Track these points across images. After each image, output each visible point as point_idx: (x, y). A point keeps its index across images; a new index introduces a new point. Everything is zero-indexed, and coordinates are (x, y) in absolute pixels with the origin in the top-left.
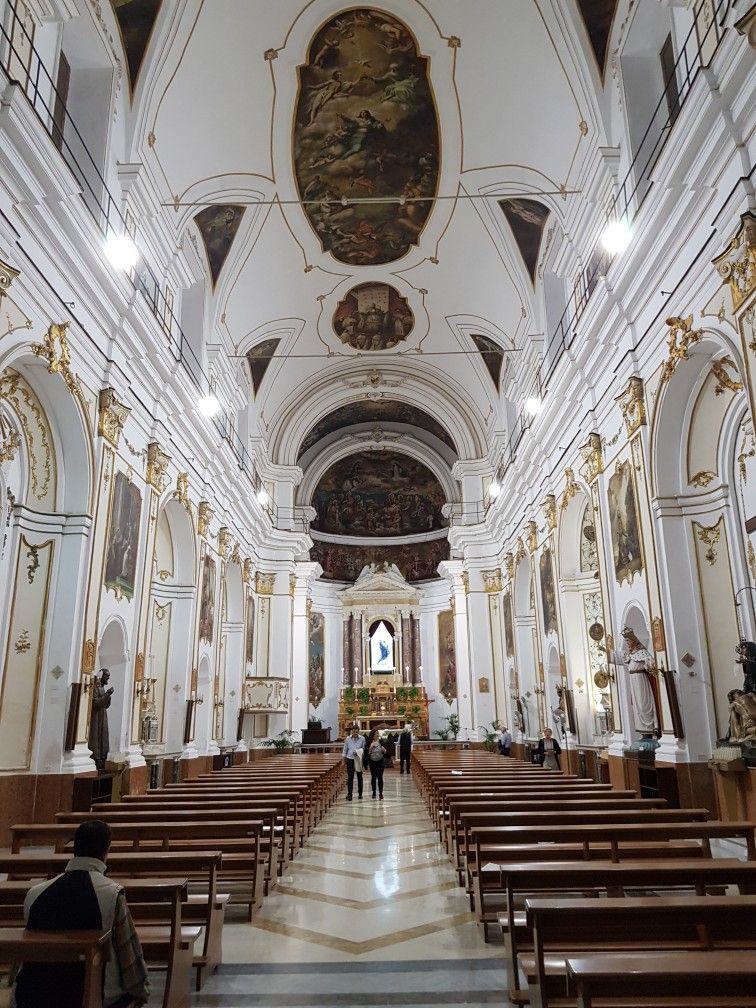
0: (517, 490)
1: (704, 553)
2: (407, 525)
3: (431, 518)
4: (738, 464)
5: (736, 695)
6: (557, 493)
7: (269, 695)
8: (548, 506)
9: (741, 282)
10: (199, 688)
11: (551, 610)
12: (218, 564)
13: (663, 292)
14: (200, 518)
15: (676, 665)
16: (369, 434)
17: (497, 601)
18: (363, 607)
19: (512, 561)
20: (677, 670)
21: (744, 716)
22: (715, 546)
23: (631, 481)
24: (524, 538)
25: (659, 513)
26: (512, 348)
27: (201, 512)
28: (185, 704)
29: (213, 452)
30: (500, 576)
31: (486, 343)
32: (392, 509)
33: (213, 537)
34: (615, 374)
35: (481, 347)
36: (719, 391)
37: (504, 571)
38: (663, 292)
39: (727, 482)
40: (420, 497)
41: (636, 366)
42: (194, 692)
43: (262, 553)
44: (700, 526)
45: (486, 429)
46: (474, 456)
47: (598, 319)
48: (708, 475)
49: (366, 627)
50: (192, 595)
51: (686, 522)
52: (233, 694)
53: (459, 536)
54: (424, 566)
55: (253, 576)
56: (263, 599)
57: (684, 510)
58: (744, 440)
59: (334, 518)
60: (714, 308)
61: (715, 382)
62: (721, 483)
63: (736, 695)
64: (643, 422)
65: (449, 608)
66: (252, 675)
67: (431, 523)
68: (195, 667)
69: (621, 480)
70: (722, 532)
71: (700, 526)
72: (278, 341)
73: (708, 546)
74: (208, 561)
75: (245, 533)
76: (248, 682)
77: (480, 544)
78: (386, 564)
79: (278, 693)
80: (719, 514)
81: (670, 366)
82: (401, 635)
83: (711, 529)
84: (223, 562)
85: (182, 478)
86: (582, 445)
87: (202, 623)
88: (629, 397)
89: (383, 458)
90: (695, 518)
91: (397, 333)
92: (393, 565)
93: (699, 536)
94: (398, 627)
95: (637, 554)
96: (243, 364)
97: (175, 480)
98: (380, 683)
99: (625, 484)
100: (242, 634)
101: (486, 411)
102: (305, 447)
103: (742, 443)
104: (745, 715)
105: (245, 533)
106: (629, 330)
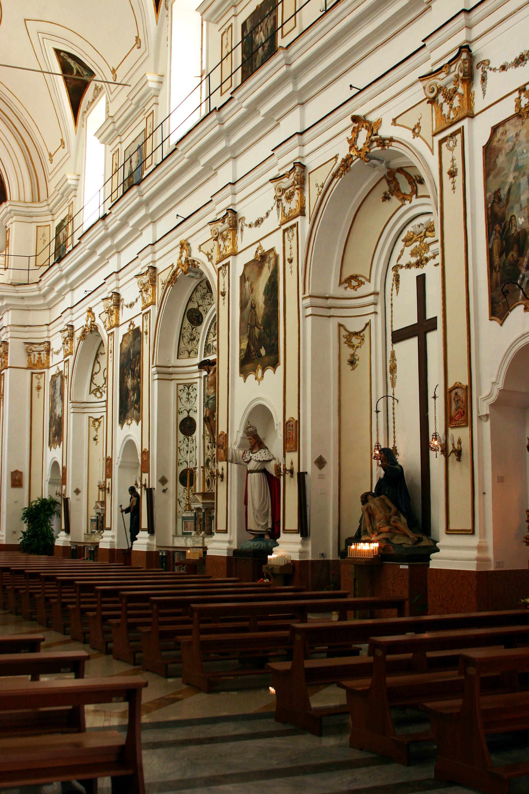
1: (346, 357)
4: (391, 274)
5: (370, 497)
6: (160, 266)
9: (446, 108)
13: (351, 86)
15: (154, 484)
17: (42, 380)
20: (155, 488)
21: (377, 517)
22: (358, 352)
23: (275, 271)
24: (97, 311)
25: (156, 376)
30: (48, 351)
31: (72, 62)
35: (66, 69)
36: (386, 198)
39: (378, 289)
44: (346, 330)
45: (50, 167)
46: (28, 198)
47: (75, 265)
48: (360, 278)
51: (333, 324)
57: (86, 410)
58: (402, 251)
60: (410, 120)
61: (384, 187)
62: (372, 290)
63: (370, 497)
64: (302, 213)
69: (261, 268)
70: (367, 339)
71: (346, 330)
73: (351, 351)
77: (28, 309)
80: (366, 319)
81: (346, 163)
83: (356, 334)
88: (286, 182)
90: (342, 321)
93: (343, 340)
95: (274, 350)
99: (266, 273)
101: (53, 145)
103: (399, 253)
104: (379, 515)
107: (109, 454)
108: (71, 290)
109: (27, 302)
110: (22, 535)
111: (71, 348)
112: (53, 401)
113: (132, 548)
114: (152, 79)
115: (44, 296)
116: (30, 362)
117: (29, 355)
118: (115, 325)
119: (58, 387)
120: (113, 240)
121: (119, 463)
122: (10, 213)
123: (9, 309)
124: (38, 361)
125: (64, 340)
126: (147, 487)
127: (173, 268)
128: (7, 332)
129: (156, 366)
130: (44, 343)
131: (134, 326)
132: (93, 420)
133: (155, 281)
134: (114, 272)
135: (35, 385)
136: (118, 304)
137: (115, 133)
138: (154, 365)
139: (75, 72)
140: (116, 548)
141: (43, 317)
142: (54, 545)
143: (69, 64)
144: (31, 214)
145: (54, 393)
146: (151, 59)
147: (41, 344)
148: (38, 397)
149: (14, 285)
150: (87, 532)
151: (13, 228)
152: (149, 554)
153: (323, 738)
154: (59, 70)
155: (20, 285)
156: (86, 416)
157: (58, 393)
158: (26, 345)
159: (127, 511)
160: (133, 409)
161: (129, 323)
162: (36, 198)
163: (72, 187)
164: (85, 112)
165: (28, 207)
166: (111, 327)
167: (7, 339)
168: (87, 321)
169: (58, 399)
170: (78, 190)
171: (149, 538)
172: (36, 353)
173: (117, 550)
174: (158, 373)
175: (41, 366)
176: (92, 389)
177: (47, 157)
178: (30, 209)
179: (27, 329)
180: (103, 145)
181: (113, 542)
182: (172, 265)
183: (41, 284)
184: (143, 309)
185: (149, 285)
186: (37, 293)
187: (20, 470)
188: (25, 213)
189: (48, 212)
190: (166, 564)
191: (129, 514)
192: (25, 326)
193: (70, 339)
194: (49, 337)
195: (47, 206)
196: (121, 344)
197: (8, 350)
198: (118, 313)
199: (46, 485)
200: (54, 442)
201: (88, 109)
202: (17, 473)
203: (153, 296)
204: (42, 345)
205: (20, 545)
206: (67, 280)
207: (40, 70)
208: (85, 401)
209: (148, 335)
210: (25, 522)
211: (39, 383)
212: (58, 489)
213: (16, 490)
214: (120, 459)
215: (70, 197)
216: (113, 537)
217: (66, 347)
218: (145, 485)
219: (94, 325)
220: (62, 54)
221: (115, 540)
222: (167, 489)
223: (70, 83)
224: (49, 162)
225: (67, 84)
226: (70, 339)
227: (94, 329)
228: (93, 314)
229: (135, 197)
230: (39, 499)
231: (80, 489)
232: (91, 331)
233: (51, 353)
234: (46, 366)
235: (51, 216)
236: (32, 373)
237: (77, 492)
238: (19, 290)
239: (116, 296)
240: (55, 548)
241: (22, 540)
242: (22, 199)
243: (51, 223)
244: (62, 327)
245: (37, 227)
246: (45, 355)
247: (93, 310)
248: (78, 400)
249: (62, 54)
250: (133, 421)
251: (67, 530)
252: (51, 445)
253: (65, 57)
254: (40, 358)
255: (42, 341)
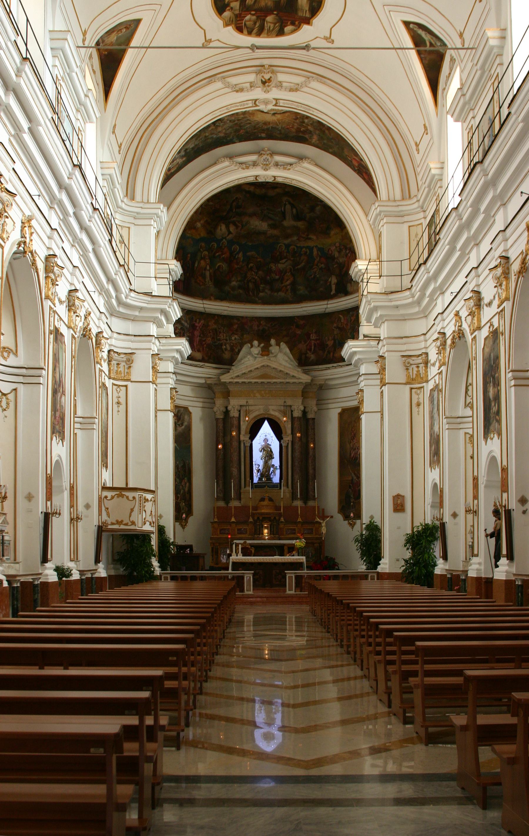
0: (458, 247)
2: (302, 290)
3: (334, 280)
6: (513, 254)
7: (132, 510)
8: (500, 270)
10: (55, 499)
11: (494, 409)
12: (67, 339)
14: (47, 277)
16: (254, 158)
17: (421, 396)
18: (242, 401)
19: (444, 344)
24: (464, 313)
25: (513, 383)
26: (460, 46)
27: (48, 270)
28: (42, 517)
29: (61, 186)
30: (426, 363)
32: (281, 266)
33: (61, 302)
34: (465, 280)
35: (418, 42)
37: (433, 356)
38: (522, 193)
40: (320, 250)
41: (506, 245)
42: (49, 503)
43: (118, 325)
45: (418, 158)
46: (398, 196)
47: (439, 264)
49: (244, 427)
50: (41, 380)
52: (88, 506)
53: (376, 308)
54: (322, 346)
55: (105, 355)
56: (119, 386)
57: (462, 426)
59: (204, 277)
65: (355, 403)
66: (109, 485)
67: (333, 287)
68: (49, 472)
72: (138, 22)
74: (57, 334)
75: (95, 296)
76: (105, 493)
77: (404, 319)
78: (273, 342)
79: (142, 509)
82: (290, 438)
84: (73, 337)
85: (27, 222)
86: (492, 265)
87: (54, 415)
89: (271, 193)
91: (300, 14)
92: (283, 345)
94: (287, 428)
96: (91, 57)
97: (19, 225)
98: (263, 500)
100: (95, 433)
101: (417, 132)
102: (168, 177)
105: (95, 296)
106: (501, 211)
107: (475, 474)
108: (440, 294)
109: (402, 312)
110: (403, 563)
111: (444, 357)
112: (432, 418)
113: (493, 577)
114: (492, 33)
115: (419, 302)
116: (408, 376)
117: (407, 369)
118: (477, 328)
119: (436, 402)
120: (469, 231)
121: (485, 483)
122: (380, 215)
123: (384, 320)
124: (416, 375)
125: (437, 349)
126: (507, 508)
127: (523, 255)
128: (384, 346)
129: (512, 371)
130: (421, 355)
131: (493, 326)
132: (469, 436)
133: (509, 273)
134: (473, 268)
135: (414, 402)
136: (479, 303)
137: (467, 107)
138: (510, 370)
139: (428, 44)
140: (483, 576)
141: (420, 326)
142: (432, 572)
143: (420, 36)
144: (402, 213)
145: (433, 408)
146: (493, 13)
147: (419, 356)
148: (418, 414)
149: (387, 294)
150: (466, 559)
151: (384, 230)
152: (508, 583)
153: (487, 811)
154: (410, 44)
155: (392, 293)
156: (462, 432)
157: (436, 409)
158: (404, 359)
159: (492, 535)
160: (495, 421)
161: (489, 324)
162: (406, 195)
163: (436, 177)
164: (444, 89)
165: (398, 206)
166: (474, 331)
167: (384, 353)
168: (455, 326)
169: (436, 416)
170: (443, 180)
171: (508, 565)
172: (414, 366)
173: (485, 578)
174: (515, 378)
175: (420, 380)
176: (467, 403)
177: (414, 147)
178: (400, 208)
179: (404, 340)
180: (459, 124)
181: (480, 570)
182: (522, 252)
183: (413, 289)
184: (499, 307)
185: (502, 278)
186: (410, 300)
187: (402, 494)
188: (396, 213)
189: (419, 209)
190: (522, 595)
191: (494, 539)
192: (402, 338)
193: (442, 348)
194: (427, 348)
195: (417, 203)
196: (483, 349)
197: (385, 365)
198: (479, 314)
199: (428, 509)
200: (434, 462)
201: (446, 86)
202: (399, 497)
203: (507, 291)
204: (420, 358)
205: (402, 573)
206: (436, 282)
207: (392, 47)
208: (460, 415)
209: (504, 336)
210: (408, 549)
211: (418, 399)
212: (436, 513)
213: (399, 515)
214: (485, 478)
215: (436, 190)
216: (480, 564)
217: (440, 358)
218: (505, 507)
219: (461, 330)
220: (411, 26)
221: (482, 567)
222: (526, 510)
223: (425, 58)
224: (416, 152)
225: (422, 60)
226: (442, 348)
227: (460, 335)
228: (460, 318)
229: (480, 177)
230: (422, 525)
231: (457, 512)
232: (459, 337)
233: (429, 364)
234: (424, 379)
235: (422, 213)
236: (411, 389)
237: (455, 515)
238: (393, 299)
239: (476, 295)
240: (434, 577)
241: (404, 567)
242: (392, 197)
243: (422, 221)
244: (436, 336)
245: (409, 227)
246: (424, 368)
247: (460, 314)
248: (453, 415)
249: (411, 26)
250: (495, 435)
251: (445, 557)
252: (432, 465)
253: (415, 29)
254: (418, 371)
255: (420, 352)
